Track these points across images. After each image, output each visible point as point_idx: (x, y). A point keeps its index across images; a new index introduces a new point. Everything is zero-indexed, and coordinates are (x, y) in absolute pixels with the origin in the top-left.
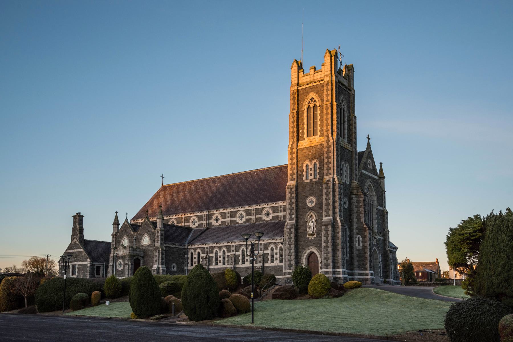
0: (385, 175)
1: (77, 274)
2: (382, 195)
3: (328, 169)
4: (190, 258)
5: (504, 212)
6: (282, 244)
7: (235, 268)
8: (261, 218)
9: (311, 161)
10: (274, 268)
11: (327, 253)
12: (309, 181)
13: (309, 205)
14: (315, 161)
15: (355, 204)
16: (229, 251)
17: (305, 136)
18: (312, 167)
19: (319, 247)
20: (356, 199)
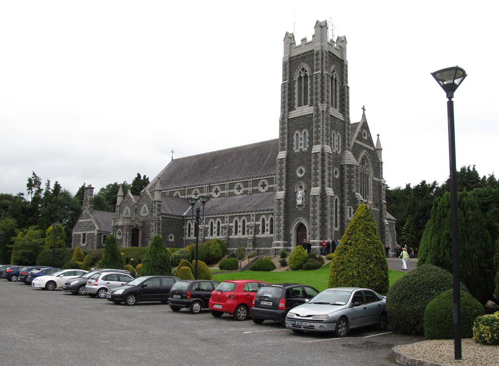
0: (383, 147)
1: (86, 242)
2: (379, 167)
3: (317, 138)
4: (188, 229)
5: (471, 169)
6: (273, 215)
7: (229, 239)
8: (257, 190)
9: (301, 130)
10: (265, 239)
11: (314, 224)
12: (298, 150)
13: (299, 175)
14: (297, 132)
15: (346, 174)
16: (249, 221)
17: (296, 106)
18: (302, 136)
19: (308, 218)
20: (348, 169)
